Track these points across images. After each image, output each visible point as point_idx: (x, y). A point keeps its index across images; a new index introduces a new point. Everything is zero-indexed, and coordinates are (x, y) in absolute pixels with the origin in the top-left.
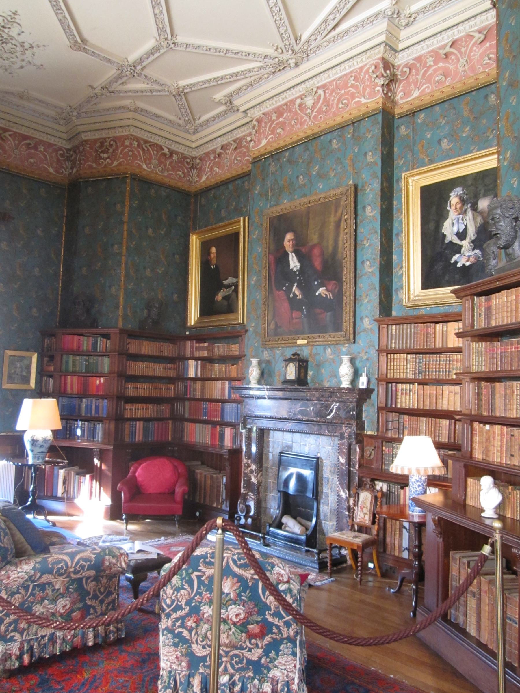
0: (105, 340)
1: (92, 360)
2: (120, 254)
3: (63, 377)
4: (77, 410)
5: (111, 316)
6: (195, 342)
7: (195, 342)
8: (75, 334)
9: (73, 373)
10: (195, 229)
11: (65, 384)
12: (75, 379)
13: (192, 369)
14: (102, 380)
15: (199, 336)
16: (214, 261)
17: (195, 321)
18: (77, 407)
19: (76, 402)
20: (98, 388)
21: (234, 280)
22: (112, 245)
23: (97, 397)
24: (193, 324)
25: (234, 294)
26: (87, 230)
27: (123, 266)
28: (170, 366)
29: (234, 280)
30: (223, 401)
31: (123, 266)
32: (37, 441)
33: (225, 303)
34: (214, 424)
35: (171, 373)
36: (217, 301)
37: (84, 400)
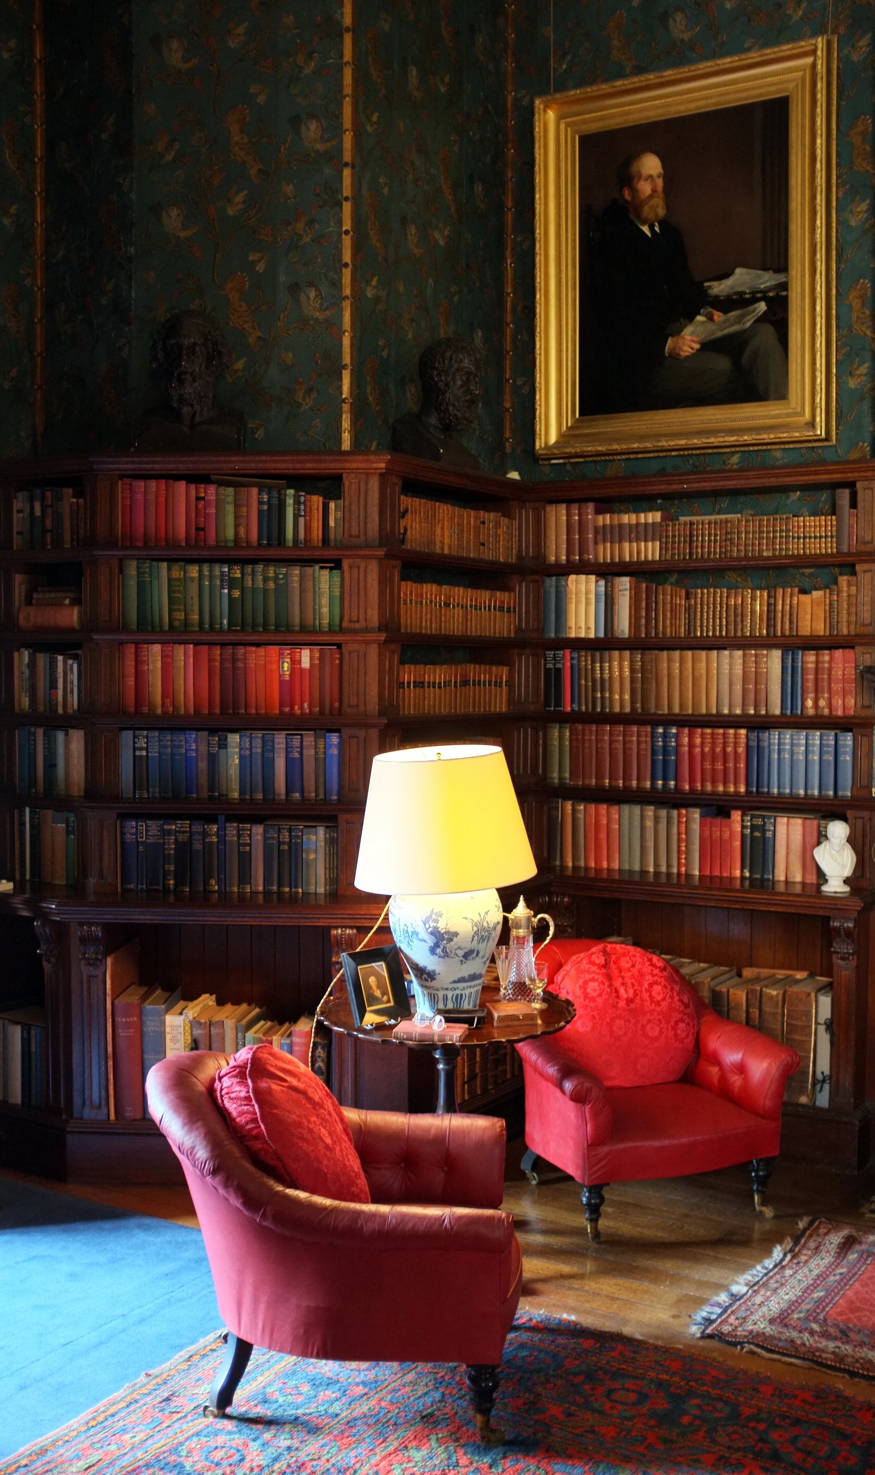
0: (317, 501)
1: (259, 578)
2: (334, 158)
3: (130, 650)
4: (203, 780)
5: (308, 404)
6: (590, 507)
7: (590, 507)
8: (177, 478)
9: (176, 634)
10: (545, 85)
11: (139, 675)
12: (183, 655)
13: (583, 607)
14: (306, 658)
15: (601, 485)
16: (657, 208)
17: (561, 435)
18: (203, 765)
19: (194, 745)
20: (288, 688)
21: (767, 280)
22: (295, 122)
23: (293, 724)
24: (553, 438)
25: (768, 332)
26: (175, 54)
27: (347, 207)
28: (485, 596)
29: (767, 280)
30: (760, 724)
31: (347, 207)
32: (452, 936)
33: (722, 364)
34: (718, 808)
35: (500, 626)
36: (674, 356)
37: (234, 739)
